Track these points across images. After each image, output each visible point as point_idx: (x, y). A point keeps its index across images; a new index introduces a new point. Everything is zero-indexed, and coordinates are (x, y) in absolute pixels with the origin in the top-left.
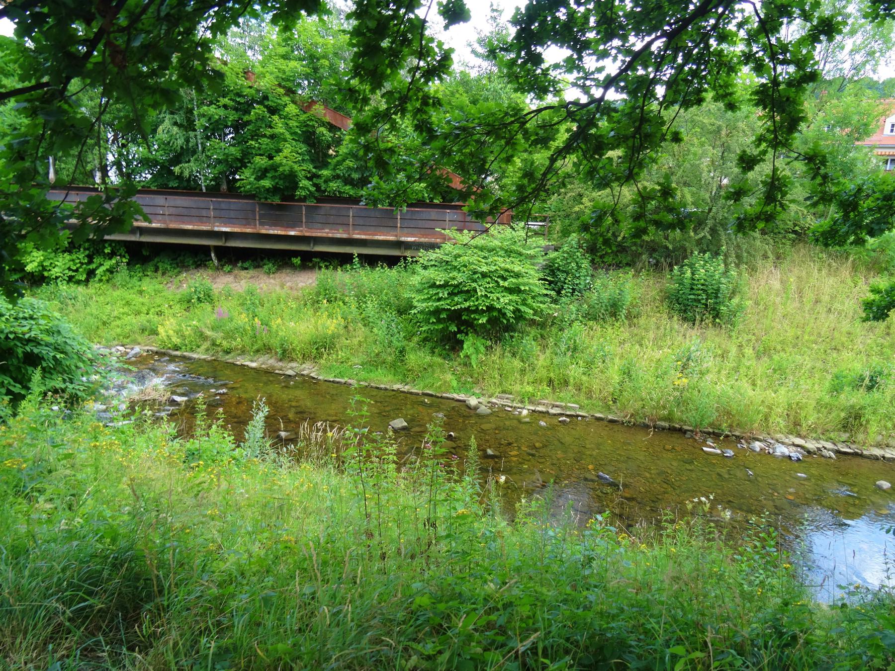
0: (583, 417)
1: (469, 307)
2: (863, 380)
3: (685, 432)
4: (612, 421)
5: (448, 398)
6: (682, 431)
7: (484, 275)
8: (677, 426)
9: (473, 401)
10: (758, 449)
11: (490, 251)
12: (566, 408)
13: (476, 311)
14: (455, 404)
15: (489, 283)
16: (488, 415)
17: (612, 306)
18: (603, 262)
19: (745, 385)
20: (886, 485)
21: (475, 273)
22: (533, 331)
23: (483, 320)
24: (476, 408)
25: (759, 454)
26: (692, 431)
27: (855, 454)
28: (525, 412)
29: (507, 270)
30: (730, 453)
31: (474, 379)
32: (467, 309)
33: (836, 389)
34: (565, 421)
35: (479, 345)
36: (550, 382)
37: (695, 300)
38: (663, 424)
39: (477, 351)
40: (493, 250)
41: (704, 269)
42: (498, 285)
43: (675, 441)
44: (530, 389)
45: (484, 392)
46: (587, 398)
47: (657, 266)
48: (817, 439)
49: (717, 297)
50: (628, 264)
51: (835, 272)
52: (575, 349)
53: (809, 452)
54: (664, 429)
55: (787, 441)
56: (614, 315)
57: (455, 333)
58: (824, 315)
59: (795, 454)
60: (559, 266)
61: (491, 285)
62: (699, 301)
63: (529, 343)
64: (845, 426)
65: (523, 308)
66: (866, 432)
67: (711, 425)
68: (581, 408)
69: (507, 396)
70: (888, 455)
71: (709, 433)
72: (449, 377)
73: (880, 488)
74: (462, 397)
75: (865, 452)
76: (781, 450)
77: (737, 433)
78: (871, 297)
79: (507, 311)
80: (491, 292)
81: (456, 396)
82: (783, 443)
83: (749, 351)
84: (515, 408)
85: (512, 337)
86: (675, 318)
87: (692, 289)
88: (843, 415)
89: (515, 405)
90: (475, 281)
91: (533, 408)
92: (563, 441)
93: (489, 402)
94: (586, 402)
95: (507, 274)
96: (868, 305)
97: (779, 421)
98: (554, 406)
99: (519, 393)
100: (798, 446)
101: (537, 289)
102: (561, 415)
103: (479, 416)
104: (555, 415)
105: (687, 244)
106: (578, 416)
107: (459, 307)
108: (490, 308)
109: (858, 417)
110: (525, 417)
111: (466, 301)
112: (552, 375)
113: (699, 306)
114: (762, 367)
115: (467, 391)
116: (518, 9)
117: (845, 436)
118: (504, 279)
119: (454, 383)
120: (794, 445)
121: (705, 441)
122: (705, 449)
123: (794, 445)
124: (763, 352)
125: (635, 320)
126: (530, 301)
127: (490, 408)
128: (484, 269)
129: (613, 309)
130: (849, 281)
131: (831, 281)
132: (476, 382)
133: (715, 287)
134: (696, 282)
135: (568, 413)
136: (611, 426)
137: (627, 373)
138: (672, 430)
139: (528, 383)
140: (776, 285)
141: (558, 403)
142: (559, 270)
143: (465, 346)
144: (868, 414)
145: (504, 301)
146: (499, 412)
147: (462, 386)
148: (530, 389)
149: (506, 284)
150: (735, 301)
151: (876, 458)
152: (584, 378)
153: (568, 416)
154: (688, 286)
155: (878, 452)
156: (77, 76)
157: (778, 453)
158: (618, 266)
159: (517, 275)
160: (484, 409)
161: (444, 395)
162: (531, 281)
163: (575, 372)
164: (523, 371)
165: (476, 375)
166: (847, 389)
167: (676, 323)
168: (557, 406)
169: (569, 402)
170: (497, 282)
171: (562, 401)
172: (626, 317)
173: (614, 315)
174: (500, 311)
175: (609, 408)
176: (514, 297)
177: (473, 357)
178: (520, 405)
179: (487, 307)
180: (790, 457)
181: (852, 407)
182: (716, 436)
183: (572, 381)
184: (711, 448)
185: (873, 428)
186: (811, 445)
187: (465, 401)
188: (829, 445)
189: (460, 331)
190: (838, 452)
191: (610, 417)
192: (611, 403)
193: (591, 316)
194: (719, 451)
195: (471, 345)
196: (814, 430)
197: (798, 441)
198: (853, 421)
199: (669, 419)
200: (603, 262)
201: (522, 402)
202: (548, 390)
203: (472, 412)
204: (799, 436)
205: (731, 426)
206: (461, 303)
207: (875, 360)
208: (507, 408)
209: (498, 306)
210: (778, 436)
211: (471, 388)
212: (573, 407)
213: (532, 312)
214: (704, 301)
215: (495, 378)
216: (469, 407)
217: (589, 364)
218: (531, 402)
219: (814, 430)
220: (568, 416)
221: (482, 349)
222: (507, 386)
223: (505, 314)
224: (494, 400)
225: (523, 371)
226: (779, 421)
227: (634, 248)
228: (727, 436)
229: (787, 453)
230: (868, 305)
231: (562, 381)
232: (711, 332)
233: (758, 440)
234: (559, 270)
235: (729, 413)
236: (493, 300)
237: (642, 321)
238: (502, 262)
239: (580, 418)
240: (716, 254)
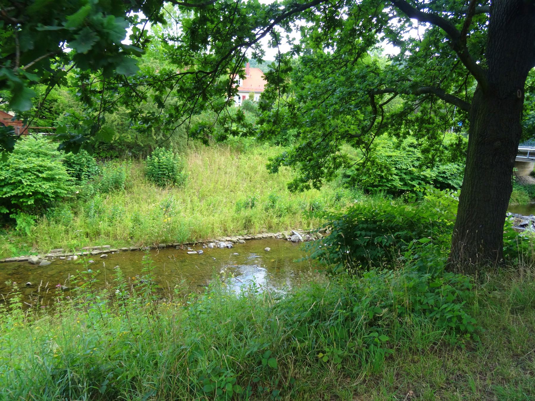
0: (115, 251)
1: (17, 194)
2: (248, 204)
3: (175, 247)
4: (133, 250)
5: (11, 261)
6: (173, 247)
7: (25, 171)
8: (170, 244)
9: (34, 259)
10: (213, 247)
11: (23, 153)
12: (102, 248)
13: (24, 196)
14: (17, 264)
15: (30, 176)
16: (49, 265)
17: (115, 183)
18: (100, 156)
19: (198, 215)
20: (268, 249)
21: (17, 170)
22: (66, 205)
23: (31, 202)
24: (38, 263)
25: (214, 249)
26: (179, 245)
27: (252, 239)
28: (75, 257)
29: (41, 166)
30: (201, 252)
31: (29, 244)
32: (16, 196)
33: (238, 210)
34: (105, 256)
35: (29, 219)
36: (87, 235)
37: (162, 174)
38: (163, 245)
39: (29, 223)
40: (26, 153)
41: (164, 156)
42: (38, 177)
43: (171, 255)
44: (75, 242)
45: (39, 251)
46: (114, 240)
47: (135, 157)
48: (235, 236)
49: (173, 171)
50: (117, 157)
51: (223, 154)
52: (100, 213)
53: (234, 242)
54: (163, 248)
55: (223, 239)
56: (117, 188)
57: (8, 214)
58: (223, 176)
59: (230, 245)
60: (74, 160)
61: (33, 177)
62: (165, 174)
63: (67, 212)
64: (245, 227)
65: (59, 190)
66: (255, 228)
67: (188, 240)
68: (112, 246)
69: (58, 250)
70: (264, 236)
71: (187, 244)
72: (8, 246)
73: (266, 251)
74: (22, 257)
75: (256, 237)
76: (223, 244)
77: (201, 241)
78: (269, 163)
79: (48, 194)
80: (33, 182)
81: (16, 258)
82: (222, 241)
83: (195, 198)
84: (67, 256)
85: (52, 211)
86: (154, 185)
87: (159, 168)
88: (244, 222)
89: (66, 254)
90: (19, 175)
91: (80, 254)
92: (110, 268)
93: (46, 257)
94: (114, 242)
95: (42, 168)
96: (269, 167)
97: (218, 231)
98: (93, 249)
99: (67, 246)
100: (229, 241)
101: (65, 177)
102: (101, 253)
103: (40, 267)
104: (96, 254)
105: (151, 143)
106: (111, 252)
107: (9, 195)
108: (35, 193)
109: (250, 221)
110: (77, 260)
111: (13, 190)
112: (88, 230)
113: (164, 177)
114: (203, 205)
115: (25, 253)
116: (276, 2)
117: (246, 232)
118: (42, 172)
119: (14, 250)
120: (227, 241)
121: (187, 249)
122: (189, 253)
123: (227, 241)
124: (202, 198)
125: (130, 190)
126: (62, 185)
127: (48, 260)
128: (25, 166)
129: (117, 184)
130: (229, 157)
131: (223, 158)
132: (32, 245)
133: (171, 166)
134: (160, 164)
135: (105, 251)
136: (133, 252)
137: (136, 220)
138: (168, 247)
139: (72, 239)
140: (200, 162)
141: (96, 247)
142: (74, 163)
143: (18, 222)
144: (253, 220)
145: (46, 187)
146: (55, 262)
147: (21, 250)
148: (75, 242)
149: (44, 175)
150: (183, 172)
151: (260, 239)
152: (110, 228)
153: (105, 253)
154: (157, 167)
155: (260, 236)
156: (171, 1)
157: (222, 246)
158: (111, 158)
159: (50, 169)
160: (45, 262)
161: (7, 259)
162: (62, 172)
163: (103, 226)
164: (67, 232)
165: (30, 241)
166: (243, 209)
167: (154, 188)
168: (96, 249)
169: (104, 245)
170: (35, 174)
171: (99, 245)
172: (125, 188)
173: (117, 188)
174: (42, 194)
175: (128, 243)
176: (51, 184)
177: (27, 228)
178: (69, 254)
179: (32, 192)
180: (227, 247)
181: (247, 217)
182: (191, 245)
183: (103, 231)
184: (191, 252)
185: (257, 225)
186: (234, 239)
187: (27, 260)
188: (241, 237)
189: (11, 213)
190: (245, 239)
191: (132, 248)
192: (130, 240)
193: (105, 190)
194: (196, 252)
195: (22, 221)
196: (233, 232)
197: (228, 239)
198: (248, 224)
199: (163, 242)
200: (100, 156)
201: (71, 251)
202: (88, 240)
203: (36, 266)
204: (228, 236)
205: (196, 238)
206: (9, 192)
207: (250, 194)
208: (61, 258)
209: (41, 191)
210: (219, 238)
211: (28, 251)
212: (107, 248)
213: (66, 192)
214: (167, 174)
215: (46, 240)
216: (32, 263)
217: (111, 220)
218: (77, 250)
219: (233, 232)
220: (105, 253)
221: (33, 222)
222: (56, 243)
223: (47, 195)
224: (50, 255)
225: (67, 232)
226: (218, 231)
227: (120, 147)
228: (196, 244)
229: (226, 246)
230: (269, 167)
231: (95, 233)
232: (174, 191)
233: (211, 242)
234: (74, 163)
235: (195, 232)
236: (36, 187)
237: (135, 189)
238: (37, 162)
239: (113, 253)
240: (167, 148)
